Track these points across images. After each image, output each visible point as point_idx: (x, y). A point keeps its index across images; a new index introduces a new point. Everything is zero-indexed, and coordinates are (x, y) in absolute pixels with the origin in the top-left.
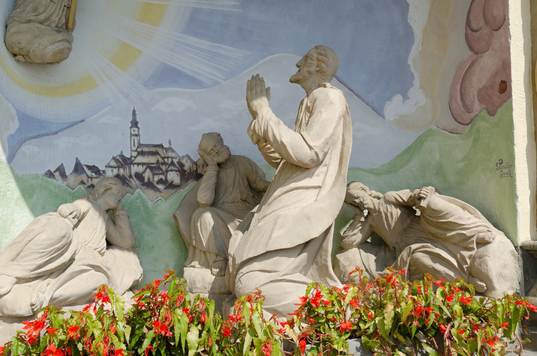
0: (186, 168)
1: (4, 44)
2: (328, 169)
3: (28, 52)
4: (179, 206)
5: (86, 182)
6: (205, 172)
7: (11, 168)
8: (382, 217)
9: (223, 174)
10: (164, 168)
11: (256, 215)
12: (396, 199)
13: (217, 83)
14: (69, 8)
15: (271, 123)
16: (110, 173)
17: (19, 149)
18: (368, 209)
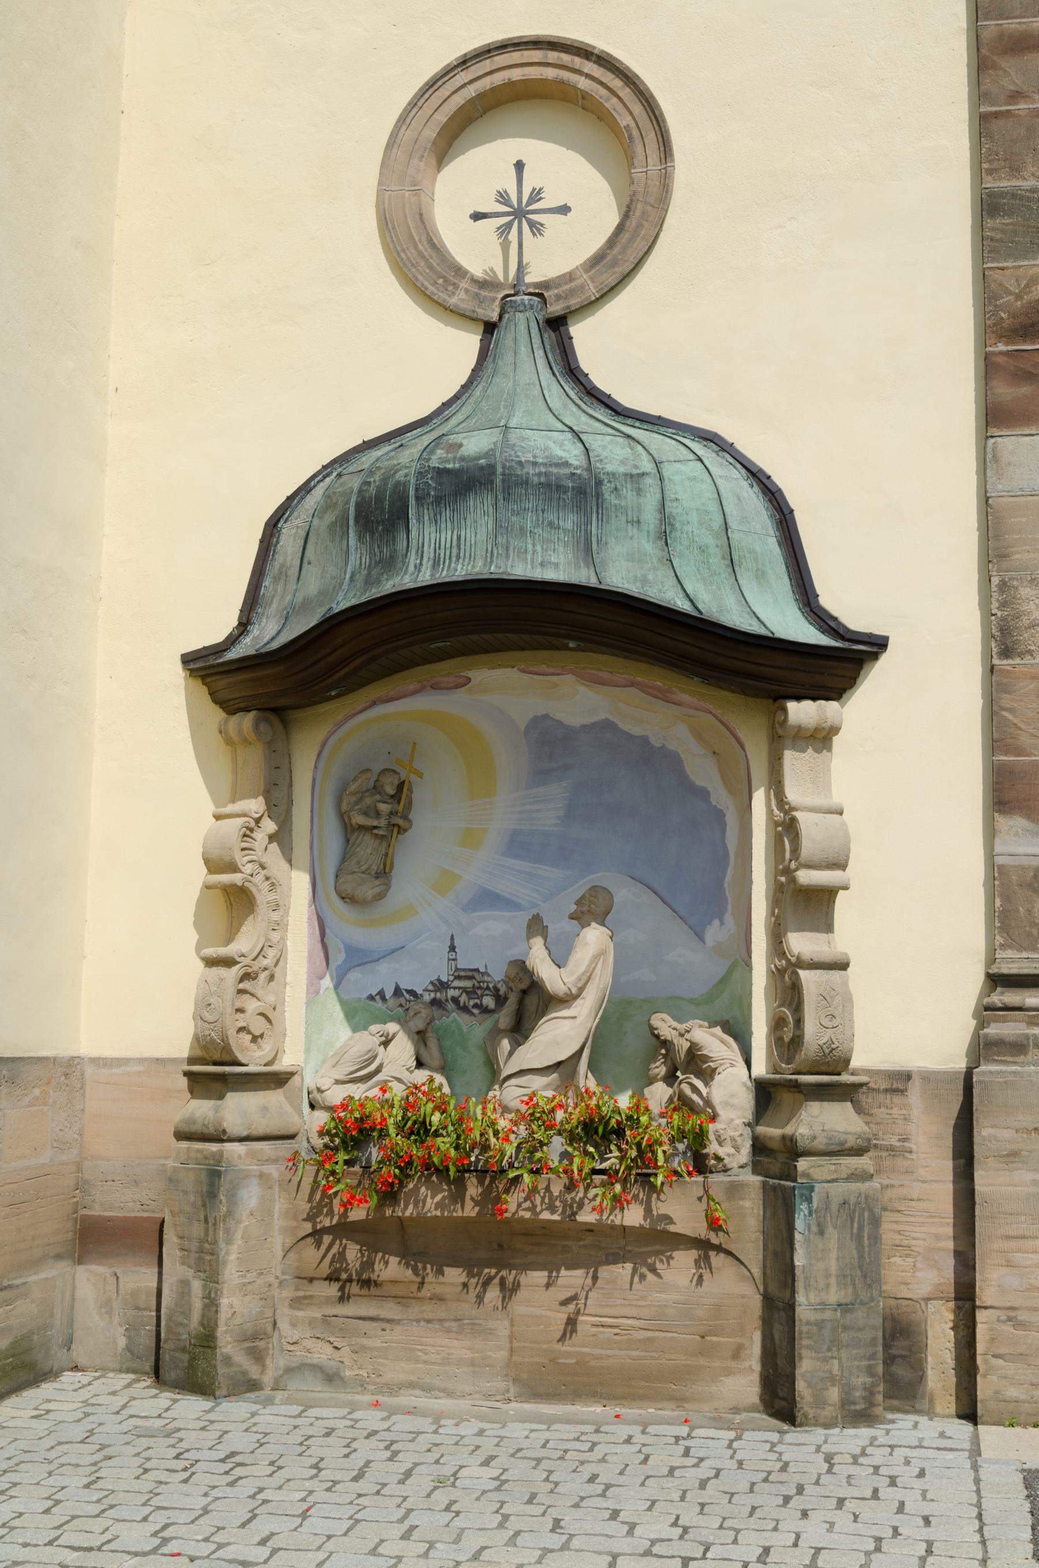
7: (338, 994)
10: (479, 992)
16: (427, 997)
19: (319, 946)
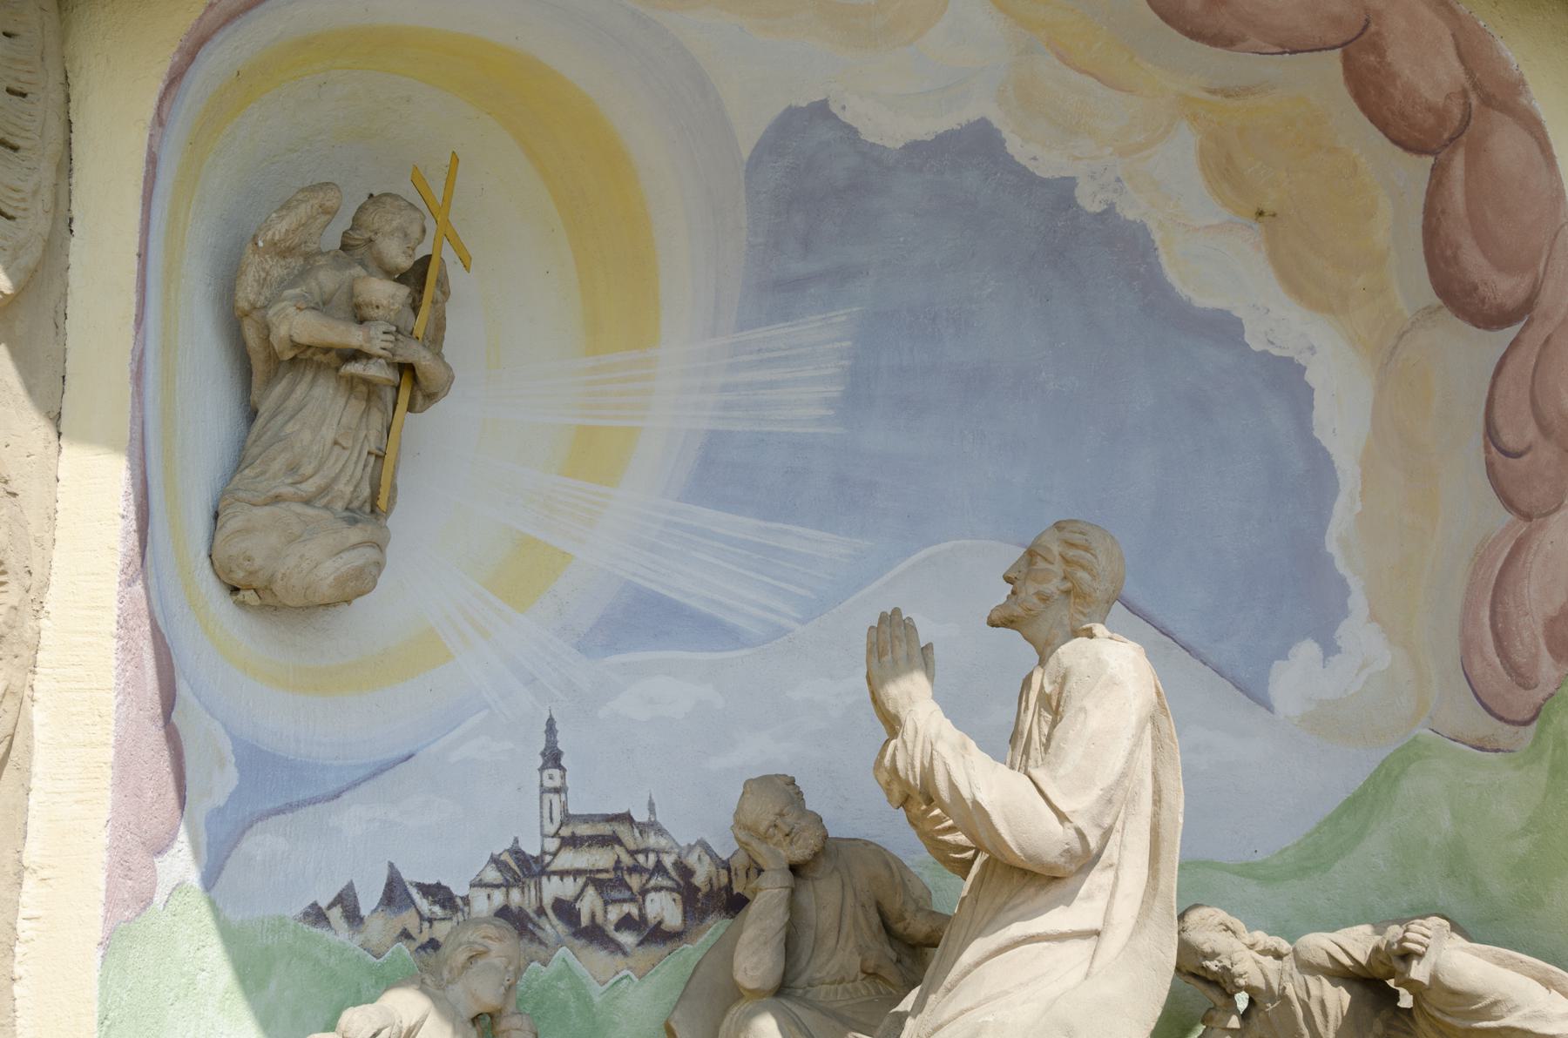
0: (699, 880)
1: (207, 563)
2: (1117, 877)
3: (271, 579)
4: (682, 997)
5: (414, 932)
6: (755, 893)
7: (213, 904)
8: (1293, 1014)
9: (806, 897)
10: (635, 881)
11: (910, 1022)
12: (1331, 956)
13: (781, 631)
14: (380, 457)
15: (943, 748)
16: (483, 904)
17: (235, 846)
18: (1248, 989)
19: (156, 734)
